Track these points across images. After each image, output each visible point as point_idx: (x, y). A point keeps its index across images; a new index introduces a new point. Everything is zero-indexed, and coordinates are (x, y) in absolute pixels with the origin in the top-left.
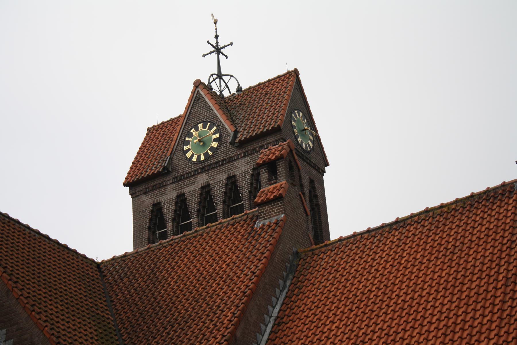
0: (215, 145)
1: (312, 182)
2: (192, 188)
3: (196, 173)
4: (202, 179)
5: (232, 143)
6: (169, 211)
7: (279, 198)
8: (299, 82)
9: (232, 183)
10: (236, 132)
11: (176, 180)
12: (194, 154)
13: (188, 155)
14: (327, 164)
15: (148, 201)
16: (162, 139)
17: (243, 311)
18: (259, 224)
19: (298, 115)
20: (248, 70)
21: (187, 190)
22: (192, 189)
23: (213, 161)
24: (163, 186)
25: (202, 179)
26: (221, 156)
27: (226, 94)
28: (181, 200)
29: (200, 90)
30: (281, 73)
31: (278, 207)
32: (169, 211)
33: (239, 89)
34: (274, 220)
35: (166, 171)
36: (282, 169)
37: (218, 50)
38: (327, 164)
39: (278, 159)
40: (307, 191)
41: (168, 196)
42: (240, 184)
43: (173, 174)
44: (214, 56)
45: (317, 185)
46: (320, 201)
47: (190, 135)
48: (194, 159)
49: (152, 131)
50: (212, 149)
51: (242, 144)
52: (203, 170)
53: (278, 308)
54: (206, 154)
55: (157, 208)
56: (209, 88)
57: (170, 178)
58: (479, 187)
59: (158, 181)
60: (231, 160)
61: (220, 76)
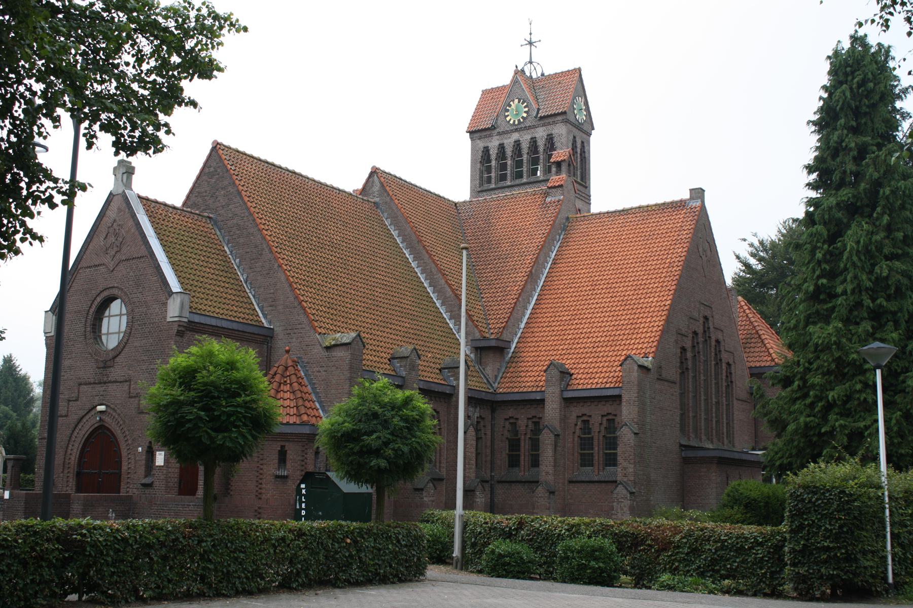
0: (525, 115)
1: (583, 142)
2: (509, 141)
3: (512, 131)
4: (515, 136)
5: (536, 117)
6: (493, 153)
7: (561, 186)
8: (580, 75)
9: (534, 141)
10: (539, 110)
11: (499, 134)
12: (511, 118)
13: (508, 119)
14: (593, 129)
15: (481, 144)
16: (491, 98)
17: (537, 258)
18: (548, 200)
19: (580, 100)
20: (550, 63)
21: (505, 142)
22: (509, 142)
23: (523, 126)
24: (490, 136)
25: (515, 136)
26: (528, 124)
27: (534, 76)
28: (502, 147)
29: (519, 72)
30: (570, 69)
31: (559, 191)
32: (493, 153)
33: (543, 75)
34: (557, 199)
35: (493, 128)
36: (564, 167)
37: (530, 43)
38: (593, 129)
39: (562, 161)
40: (579, 150)
41: (493, 144)
42: (538, 144)
43: (498, 130)
44: (528, 46)
45: (585, 144)
46: (587, 155)
47: (510, 106)
48: (511, 122)
49: (485, 93)
50: (523, 117)
51: (541, 118)
52: (516, 130)
53: (554, 253)
54: (519, 120)
55: (486, 150)
56: (523, 71)
57: (496, 132)
58: (668, 199)
59: (488, 133)
60: (534, 127)
61: (531, 62)
